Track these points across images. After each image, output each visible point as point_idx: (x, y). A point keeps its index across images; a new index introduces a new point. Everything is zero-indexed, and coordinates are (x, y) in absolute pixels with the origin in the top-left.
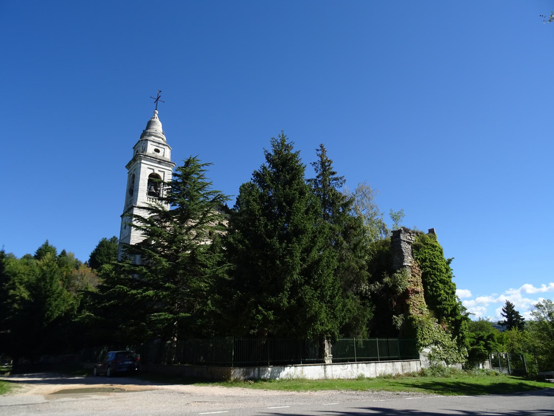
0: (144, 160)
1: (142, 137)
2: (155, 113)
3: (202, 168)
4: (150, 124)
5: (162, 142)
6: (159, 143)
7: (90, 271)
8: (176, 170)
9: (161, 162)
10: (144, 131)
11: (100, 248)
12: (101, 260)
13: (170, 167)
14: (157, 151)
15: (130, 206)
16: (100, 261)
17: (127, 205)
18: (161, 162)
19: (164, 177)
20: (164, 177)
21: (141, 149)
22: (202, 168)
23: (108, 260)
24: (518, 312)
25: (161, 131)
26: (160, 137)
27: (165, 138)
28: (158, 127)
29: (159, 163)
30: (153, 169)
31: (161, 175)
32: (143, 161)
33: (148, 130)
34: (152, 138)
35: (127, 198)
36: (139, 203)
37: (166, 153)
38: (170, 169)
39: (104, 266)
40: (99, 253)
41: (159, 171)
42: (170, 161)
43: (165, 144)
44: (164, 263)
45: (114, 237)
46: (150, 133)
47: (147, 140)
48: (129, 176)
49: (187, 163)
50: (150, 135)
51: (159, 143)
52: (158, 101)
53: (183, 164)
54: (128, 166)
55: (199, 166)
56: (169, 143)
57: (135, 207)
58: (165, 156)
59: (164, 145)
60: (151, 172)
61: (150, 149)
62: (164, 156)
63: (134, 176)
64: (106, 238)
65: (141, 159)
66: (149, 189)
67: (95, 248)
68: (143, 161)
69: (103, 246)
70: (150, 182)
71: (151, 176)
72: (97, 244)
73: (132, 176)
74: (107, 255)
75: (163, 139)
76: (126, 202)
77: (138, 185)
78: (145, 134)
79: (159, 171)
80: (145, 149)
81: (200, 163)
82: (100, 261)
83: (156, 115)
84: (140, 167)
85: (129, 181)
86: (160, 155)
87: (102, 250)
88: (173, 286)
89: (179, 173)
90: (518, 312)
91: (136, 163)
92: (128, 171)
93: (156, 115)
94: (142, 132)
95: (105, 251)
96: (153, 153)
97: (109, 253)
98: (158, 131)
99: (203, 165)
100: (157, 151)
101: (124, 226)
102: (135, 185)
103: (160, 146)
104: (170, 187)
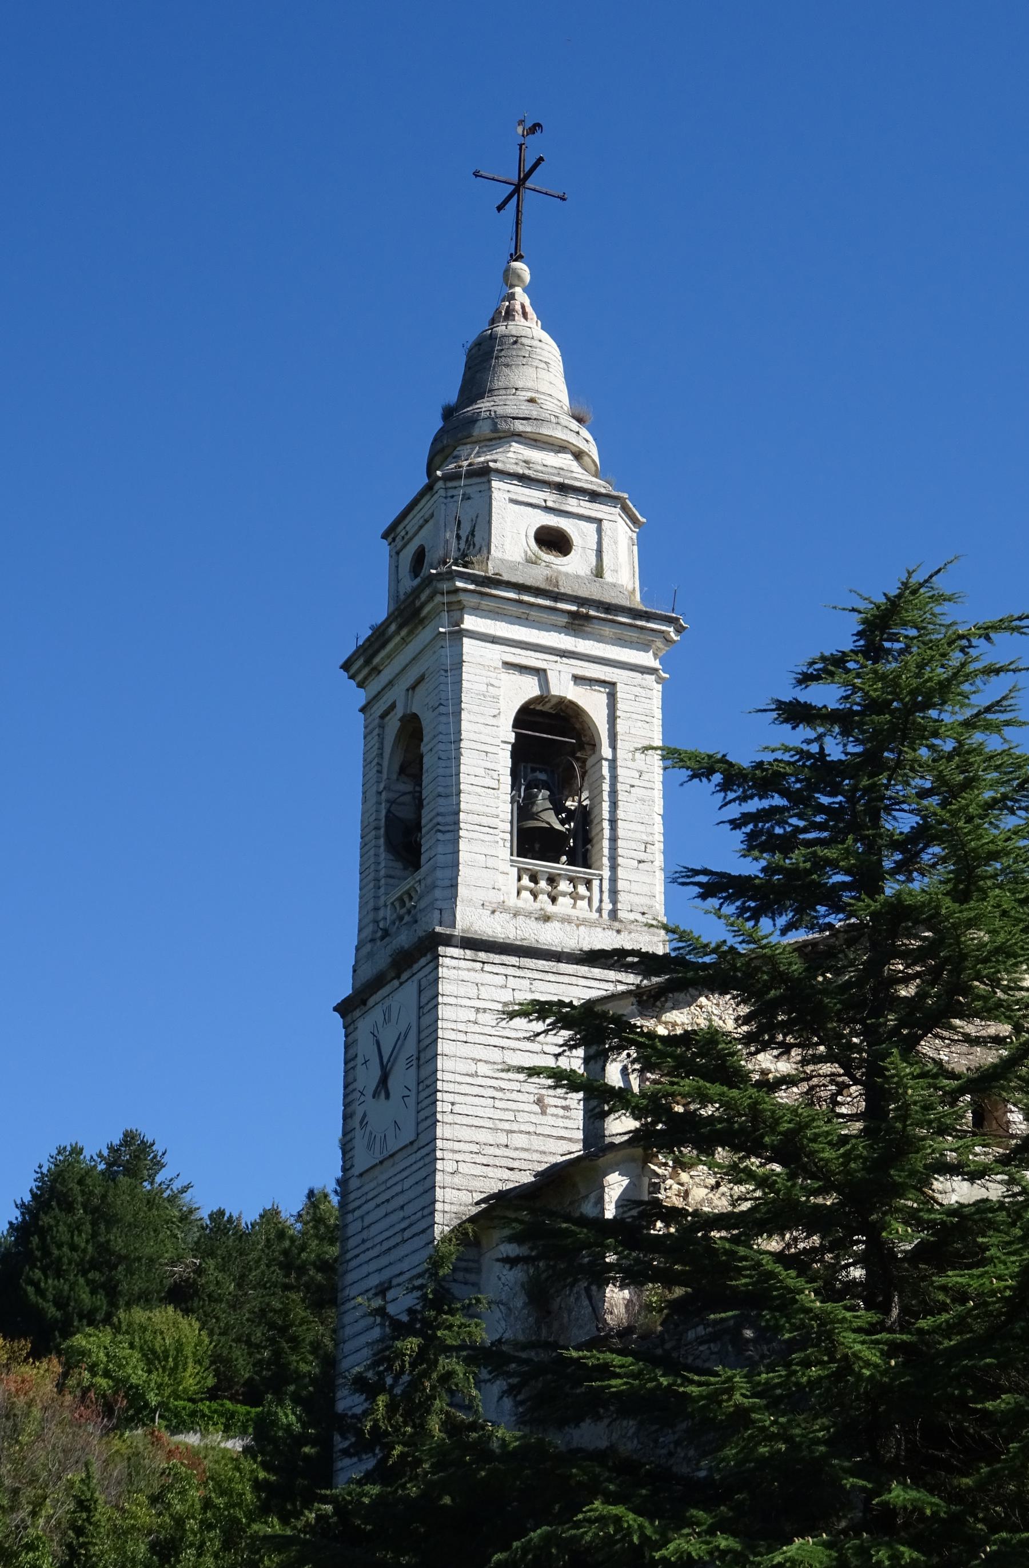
0: (477, 611)
1: (441, 450)
2: (509, 278)
3: (984, 653)
4: (485, 359)
5: (580, 476)
6: (563, 489)
7: (49, 1387)
8: (805, 679)
9: (584, 615)
10: (448, 413)
11: (45, 1220)
12: (61, 1303)
13: (645, 647)
14: (553, 541)
15: (404, 939)
16: (52, 1311)
17: (374, 932)
18: (584, 615)
19: (612, 719)
20: (612, 719)
21: (450, 535)
22: (984, 653)
23: (101, 1300)
24: (22, 1206)
25: (564, 397)
26: (561, 447)
27: (593, 450)
28: (540, 376)
29: (577, 623)
30: (540, 673)
31: (593, 705)
32: (470, 622)
33: (484, 405)
34: (513, 456)
35: (371, 883)
36: (471, 916)
37: (611, 554)
38: (647, 659)
39: (79, 1340)
40: (46, 1253)
41: (578, 679)
42: (637, 602)
43: (599, 485)
44: (853, 1343)
45: (129, 1138)
46: (494, 420)
47: (485, 472)
48: (374, 731)
49: (879, 625)
50: (501, 435)
51: (563, 489)
52: (527, 196)
53: (842, 636)
54: (364, 661)
55: (961, 641)
56: (625, 481)
57: (448, 941)
58: (609, 576)
59: (594, 496)
60: (529, 689)
61: (511, 531)
62: (599, 572)
63: (412, 730)
64: (77, 1151)
65: (457, 609)
66: (523, 810)
67: (15, 1215)
68: (470, 622)
69: (69, 1207)
70: (523, 754)
71: (528, 717)
72: (24, 1188)
73: (393, 724)
74: (94, 1265)
75: (578, 455)
76: (370, 909)
77: (453, 792)
78: (464, 431)
79: (578, 679)
80: (475, 538)
81: (959, 616)
82: (52, 1311)
83: (521, 297)
84: (458, 664)
85: (372, 762)
86: (573, 568)
87: (62, 1232)
88: (931, 1503)
89: (826, 695)
90: (22, 1206)
91: (424, 636)
92: (361, 697)
93: (521, 297)
94: (437, 423)
95: (80, 1241)
96: (531, 561)
97: (104, 1248)
98: (550, 405)
99: (986, 632)
100: (553, 541)
101: (368, 1077)
102: (427, 791)
103: (572, 504)
104: (778, 801)
